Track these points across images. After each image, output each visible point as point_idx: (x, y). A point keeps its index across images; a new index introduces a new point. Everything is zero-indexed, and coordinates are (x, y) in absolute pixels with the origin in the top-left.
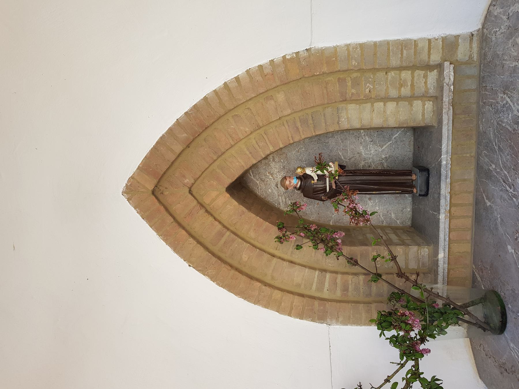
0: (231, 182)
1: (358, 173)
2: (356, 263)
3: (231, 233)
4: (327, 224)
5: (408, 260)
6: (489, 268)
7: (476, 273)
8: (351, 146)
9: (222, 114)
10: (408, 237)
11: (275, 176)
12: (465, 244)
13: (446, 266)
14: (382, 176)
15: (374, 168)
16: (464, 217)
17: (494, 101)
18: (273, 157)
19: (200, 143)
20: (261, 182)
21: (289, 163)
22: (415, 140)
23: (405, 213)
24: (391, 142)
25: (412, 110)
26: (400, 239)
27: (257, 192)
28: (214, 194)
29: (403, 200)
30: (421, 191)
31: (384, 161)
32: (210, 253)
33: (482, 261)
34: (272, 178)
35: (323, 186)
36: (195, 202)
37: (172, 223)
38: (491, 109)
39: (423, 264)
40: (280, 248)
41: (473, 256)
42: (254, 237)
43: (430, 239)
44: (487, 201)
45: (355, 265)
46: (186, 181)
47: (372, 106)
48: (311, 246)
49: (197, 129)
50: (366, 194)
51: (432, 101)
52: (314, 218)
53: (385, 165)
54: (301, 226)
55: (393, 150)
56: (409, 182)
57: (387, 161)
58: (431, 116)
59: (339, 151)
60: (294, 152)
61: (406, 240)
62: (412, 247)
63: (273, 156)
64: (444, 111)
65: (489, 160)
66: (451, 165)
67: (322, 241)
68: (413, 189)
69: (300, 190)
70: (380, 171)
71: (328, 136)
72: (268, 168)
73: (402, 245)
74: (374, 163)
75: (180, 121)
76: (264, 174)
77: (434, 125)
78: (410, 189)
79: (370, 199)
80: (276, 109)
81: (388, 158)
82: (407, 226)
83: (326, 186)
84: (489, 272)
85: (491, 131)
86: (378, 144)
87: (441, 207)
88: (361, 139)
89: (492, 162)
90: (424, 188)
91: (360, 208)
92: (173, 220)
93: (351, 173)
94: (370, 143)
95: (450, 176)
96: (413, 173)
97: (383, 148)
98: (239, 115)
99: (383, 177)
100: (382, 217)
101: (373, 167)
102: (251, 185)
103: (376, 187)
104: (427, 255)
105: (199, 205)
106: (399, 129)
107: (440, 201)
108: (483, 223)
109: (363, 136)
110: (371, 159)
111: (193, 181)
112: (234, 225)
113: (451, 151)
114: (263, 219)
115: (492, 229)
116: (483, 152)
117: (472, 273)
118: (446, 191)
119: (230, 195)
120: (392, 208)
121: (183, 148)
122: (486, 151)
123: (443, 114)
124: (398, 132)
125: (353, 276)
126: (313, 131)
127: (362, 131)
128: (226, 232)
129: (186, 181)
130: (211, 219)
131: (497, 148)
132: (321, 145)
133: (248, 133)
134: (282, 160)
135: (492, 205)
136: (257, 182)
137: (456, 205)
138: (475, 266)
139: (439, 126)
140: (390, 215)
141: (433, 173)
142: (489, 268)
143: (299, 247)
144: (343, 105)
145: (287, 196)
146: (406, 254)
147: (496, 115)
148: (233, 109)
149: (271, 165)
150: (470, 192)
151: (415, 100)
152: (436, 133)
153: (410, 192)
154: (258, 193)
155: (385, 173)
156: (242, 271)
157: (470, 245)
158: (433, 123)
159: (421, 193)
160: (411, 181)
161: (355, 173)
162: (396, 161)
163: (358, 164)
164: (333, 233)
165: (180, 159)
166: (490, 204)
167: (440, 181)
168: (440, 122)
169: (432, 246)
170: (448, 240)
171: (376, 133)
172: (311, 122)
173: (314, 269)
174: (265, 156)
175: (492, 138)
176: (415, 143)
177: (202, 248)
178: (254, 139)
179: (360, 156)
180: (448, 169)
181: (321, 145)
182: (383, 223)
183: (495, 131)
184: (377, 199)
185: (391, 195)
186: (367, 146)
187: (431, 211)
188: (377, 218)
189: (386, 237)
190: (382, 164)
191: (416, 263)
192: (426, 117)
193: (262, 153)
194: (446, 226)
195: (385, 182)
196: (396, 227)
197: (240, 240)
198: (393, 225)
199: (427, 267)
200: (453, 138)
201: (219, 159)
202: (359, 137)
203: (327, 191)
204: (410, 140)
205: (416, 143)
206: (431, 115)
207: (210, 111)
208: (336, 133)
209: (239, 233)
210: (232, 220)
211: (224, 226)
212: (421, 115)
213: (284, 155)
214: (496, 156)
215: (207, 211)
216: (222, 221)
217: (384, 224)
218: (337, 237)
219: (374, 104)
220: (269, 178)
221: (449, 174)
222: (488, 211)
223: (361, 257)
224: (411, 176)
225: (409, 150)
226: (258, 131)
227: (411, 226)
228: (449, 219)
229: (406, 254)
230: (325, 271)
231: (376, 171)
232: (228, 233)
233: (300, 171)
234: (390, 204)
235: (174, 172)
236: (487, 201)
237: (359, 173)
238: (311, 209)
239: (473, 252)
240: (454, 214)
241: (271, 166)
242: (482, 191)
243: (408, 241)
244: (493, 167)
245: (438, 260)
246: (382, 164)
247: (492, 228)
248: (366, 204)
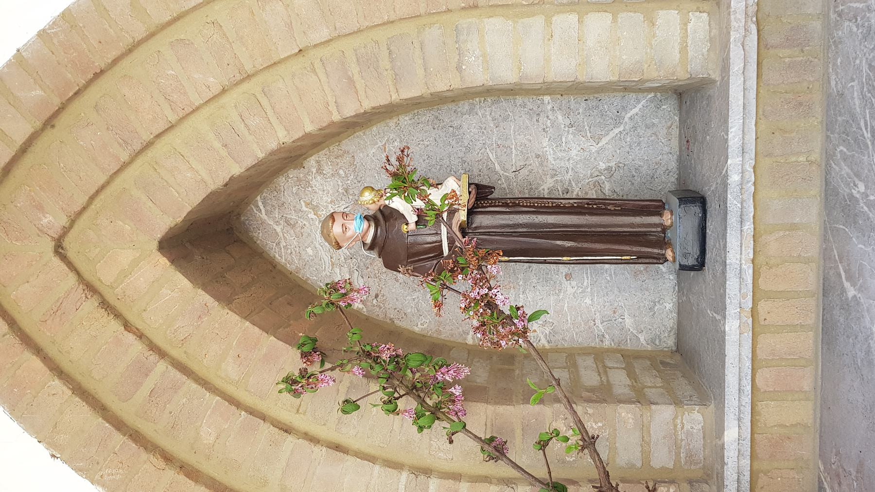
0: (172, 225)
1: (523, 206)
2: (497, 454)
3: (169, 366)
4: (460, 340)
5: (649, 444)
6: (854, 473)
7: (825, 483)
8: (518, 137)
9: (139, 37)
10: (659, 380)
12: (796, 403)
13: (746, 462)
15: (578, 195)
16: (793, 328)
17: (862, 5)
18: (318, 162)
19: (83, 114)
21: (359, 178)
22: (682, 122)
23: (660, 314)
24: (621, 129)
25: (654, 36)
26: (635, 384)
27: (277, 256)
28: (126, 257)
29: (653, 279)
30: (685, 255)
31: (603, 177)
32: (108, 422)
33: (838, 454)
34: (314, 217)
35: (434, 238)
36: (72, 278)
37: (4, 336)
38: (855, 29)
39: (690, 456)
40: (307, 408)
41: (818, 436)
42: (237, 379)
43: (708, 387)
44: (847, 285)
45: (496, 459)
46: (46, 220)
47: (548, 22)
48: (378, 405)
49: (70, 76)
51: (709, 13)
52: (425, 326)
54: (357, 349)
55: (628, 149)
56: (654, 232)
58: (706, 53)
59: (488, 150)
60: (374, 151)
61: (650, 387)
62: (658, 407)
64: (734, 36)
65: (852, 170)
67: (413, 390)
68: (664, 252)
69: (375, 250)
70: (581, 203)
71: (459, 110)
72: (304, 191)
73: (634, 403)
75: (24, 54)
76: (295, 207)
77: (713, 77)
78: (656, 251)
79: (568, 277)
80: (290, 26)
81: (614, 169)
82: (666, 349)
83: (441, 241)
84: (855, 484)
85: (855, 89)
86: (588, 132)
87: (728, 301)
89: (858, 175)
90: (695, 251)
91: (505, 300)
92: (7, 327)
93: (506, 205)
96: (666, 207)
97: (600, 145)
98: (189, 40)
99: (588, 217)
100: (600, 326)
101: (575, 193)
102: (260, 237)
103: (568, 244)
104: (700, 430)
105: (81, 286)
106: (640, 95)
108: (839, 346)
110: (570, 172)
111: (64, 221)
113: (753, 147)
114: (261, 327)
115: (859, 364)
116: (838, 150)
117: (817, 484)
119: (172, 262)
121: (33, 127)
122: (844, 147)
123: (731, 46)
124: (639, 101)
125: (500, 487)
126: (392, 88)
127: (547, 98)
128: (156, 364)
129: (46, 220)
130: (115, 326)
131: (869, 135)
132: (441, 134)
133: (213, 92)
134: (341, 172)
135: (860, 295)
136: (275, 227)
137: (771, 296)
138: (824, 464)
139: (723, 79)
140: (620, 320)
142: (855, 473)
143: (350, 406)
144: (466, 21)
145: (355, 268)
146: (644, 429)
147: (866, 43)
148: (169, 23)
149: (313, 183)
150: (807, 261)
151: (662, 9)
153: (659, 259)
155: (595, 206)
156: (198, 471)
157: (810, 405)
158: (711, 72)
159: (685, 262)
160: (659, 229)
162: (636, 178)
165: (28, 160)
166: (854, 292)
168: (725, 68)
169: (712, 406)
170: (750, 392)
171: (583, 104)
172: (385, 63)
173: (397, 466)
174: (264, 155)
175: (858, 110)
176: (682, 131)
177: (86, 408)
178: (235, 106)
179: (541, 164)
180: (745, 197)
181: (441, 134)
182: (602, 341)
183: (865, 89)
184: (585, 278)
185: (622, 266)
186: (561, 139)
190: (598, 185)
191: (670, 452)
192: (690, 54)
193: (255, 145)
194: (743, 354)
195: (594, 232)
196: (638, 351)
197: (194, 386)
198: (629, 347)
199: (701, 465)
200: (761, 112)
201: (139, 161)
202: (538, 114)
203: (443, 254)
204: (669, 124)
205: (684, 130)
206: (705, 51)
207: (107, 26)
208: (480, 102)
209: (194, 366)
210: (176, 331)
211: (153, 347)
212: (677, 51)
213: (347, 159)
214: (866, 157)
215: (105, 305)
216: (147, 333)
217: (607, 344)
218: (447, 378)
219: (554, 18)
220: (308, 219)
222: (850, 314)
223: (523, 435)
224: (660, 215)
225: (666, 149)
226: (245, 86)
227: (674, 348)
229: (644, 429)
230: (427, 472)
231: (571, 201)
232: (162, 366)
233: (370, 198)
234: (620, 292)
235: (13, 196)
236: (847, 285)
237: (526, 206)
238: (416, 300)
239: (818, 425)
240: (765, 319)
241: (312, 187)
242: (837, 257)
243: (654, 390)
244: (860, 189)
245: (722, 447)
246: (598, 185)
247: (859, 360)
248: (560, 291)
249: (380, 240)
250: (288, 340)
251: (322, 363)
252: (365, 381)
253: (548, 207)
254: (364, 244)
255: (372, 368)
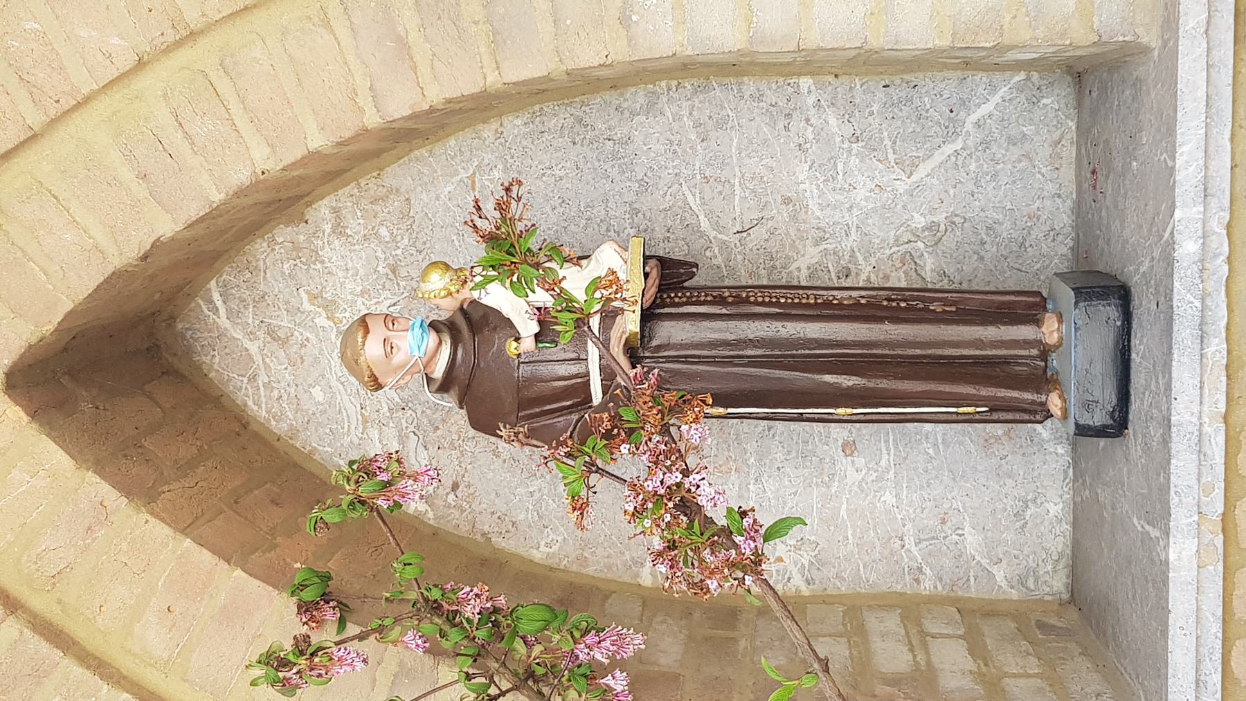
1: (756, 303)
8: (747, 161)
11: (347, 315)
14: (880, 320)
15: (868, 280)
18: (336, 211)
20: (275, 346)
21: (419, 245)
22: (1083, 132)
24: (958, 145)
27: (250, 403)
30: (1087, 406)
34: (327, 323)
35: (573, 369)
42: (165, 656)
50: (800, 418)
53: (928, 268)
54: (413, 595)
55: (971, 186)
57: (936, 244)
60: (450, 188)
61: (1015, 676)
63: (334, 204)
66: (1229, 260)
71: (625, 105)
74: (868, 254)
76: (287, 303)
78: (1028, 396)
79: (849, 448)
81: (942, 227)
82: (1050, 598)
83: (587, 375)
86: (890, 151)
87: (1174, 500)
88: (803, 124)
90: (1107, 396)
93: (721, 301)
94: (846, 146)
95: (1224, 323)
96: (1049, 306)
97: (915, 178)
100: (914, 549)
101: (863, 277)
102: (216, 364)
106: (998, 77)
107: (1169, 463)
109: (813, 111)
112: (54, 584)
118: (1205, 408)
119: (34, 415)
120: (967, 498)
124: (994, 89)
127: (806, 82)
132: (590, 154)
134: (383, 231)
136: (248, 344)
139: (1165, 43)
141: (1143, 305)
149: (326, 253)
152: (1155, 86)
154: (256, 408)
155: (903, 304)
158: (1140, 31)
159: (1086, 420)
160: (1035, 352)
161: (739, 301)
163: (787, 257)
164: (577, 634)
167: (1170, 348)
168: (1170, 24)
170: (1219, 686)
171: (880, 94)
174: (222, 196)
176: (1083, 151)
178: (165, 96)
179: (794, 218)
181: (590, 154)
182: (917, 580)
184: (884, 451)
186: (835, 165)
187: (1139, 519)
188: (887, 552)
189: (915, 656)
190: (910, 259)
202: (788, 115)
204: (1057, 135)
208: (669, 89)
213: (395, 204)
217: (928, 586)
220: (314, 328)
221: (1220, 314)
224: (1037, 322)
225: (1051, 188)
226: (184, 56)
227: (1066, 596)
228: (1221, 568)
231: (855, 294)
233: (440, 285)
237: (763, 304)
238: (536, 496)
241: (322, 262)
246: (910, 259)
249: (462, 373)
250: (272, 577)
251: (342, 623)
252: (429, 661)
253: (808, 306)
254: (429, 380)
255: (443, 635)
